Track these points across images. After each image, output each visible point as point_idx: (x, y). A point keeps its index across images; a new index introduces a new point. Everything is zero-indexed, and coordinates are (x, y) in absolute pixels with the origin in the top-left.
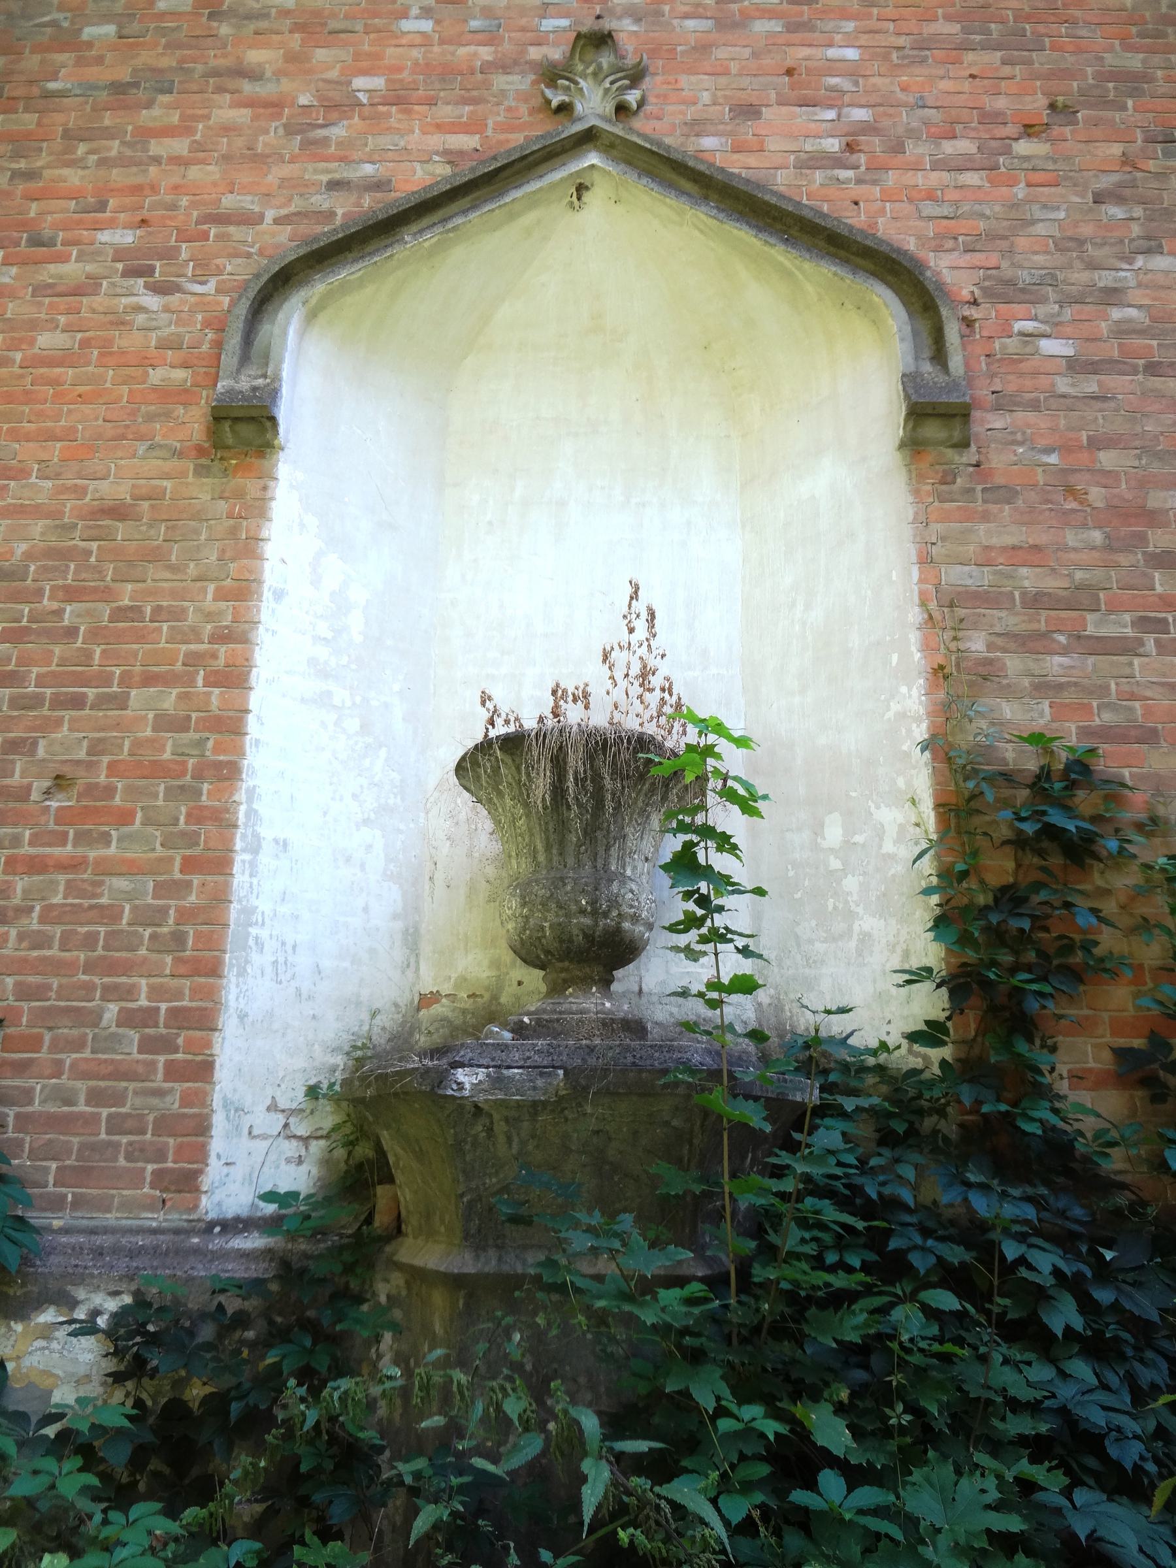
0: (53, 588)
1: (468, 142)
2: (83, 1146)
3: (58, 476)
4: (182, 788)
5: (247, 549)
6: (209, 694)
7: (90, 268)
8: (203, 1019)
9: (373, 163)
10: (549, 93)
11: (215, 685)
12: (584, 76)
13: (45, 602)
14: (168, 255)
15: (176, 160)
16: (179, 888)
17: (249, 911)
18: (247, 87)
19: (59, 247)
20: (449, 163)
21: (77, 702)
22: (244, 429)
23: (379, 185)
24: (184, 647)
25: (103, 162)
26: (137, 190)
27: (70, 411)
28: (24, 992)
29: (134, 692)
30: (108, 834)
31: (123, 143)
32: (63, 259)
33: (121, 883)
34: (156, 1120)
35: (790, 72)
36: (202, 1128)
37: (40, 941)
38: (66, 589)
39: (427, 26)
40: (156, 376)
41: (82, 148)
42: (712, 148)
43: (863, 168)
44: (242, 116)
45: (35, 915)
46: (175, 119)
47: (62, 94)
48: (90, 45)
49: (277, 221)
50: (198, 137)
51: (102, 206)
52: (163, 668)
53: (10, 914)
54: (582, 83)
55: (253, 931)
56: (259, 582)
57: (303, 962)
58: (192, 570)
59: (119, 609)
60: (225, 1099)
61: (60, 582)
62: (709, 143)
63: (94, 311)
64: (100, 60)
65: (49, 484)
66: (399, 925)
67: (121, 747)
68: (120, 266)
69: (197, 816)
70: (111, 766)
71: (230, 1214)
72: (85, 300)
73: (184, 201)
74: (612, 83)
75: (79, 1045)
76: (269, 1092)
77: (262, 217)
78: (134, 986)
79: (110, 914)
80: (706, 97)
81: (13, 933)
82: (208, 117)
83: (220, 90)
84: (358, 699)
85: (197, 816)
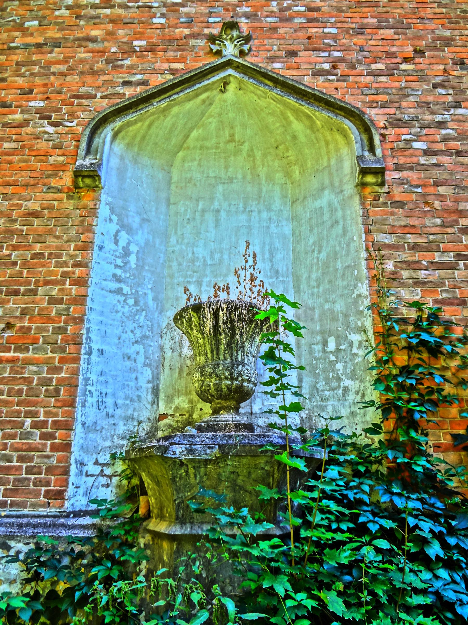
0: (7, 246)
4: (59, 328)
10: (212, 46)
14: (58, 111)
18: (91, 45)
21: (16, 292)
22: (88, 179)
23: (144, 83)
24: (61, 270)
27: (16, 174)
32: (15, 113)
38: (13, 246)
39: (163, 21)
41: (23, 69)
49: (102, 97)
51: (31, 92)
52: (52, 278)
60: (76, 459)
61: (11, 243)
64: (32, 35)
68: (38, 115)
70: (30, 319)
72: (23, 129)
75: (13, 437)
77: (96, 95)
78: (38, 411)
79: (28, 381)
83: (80, 46)
84: (133, 291)
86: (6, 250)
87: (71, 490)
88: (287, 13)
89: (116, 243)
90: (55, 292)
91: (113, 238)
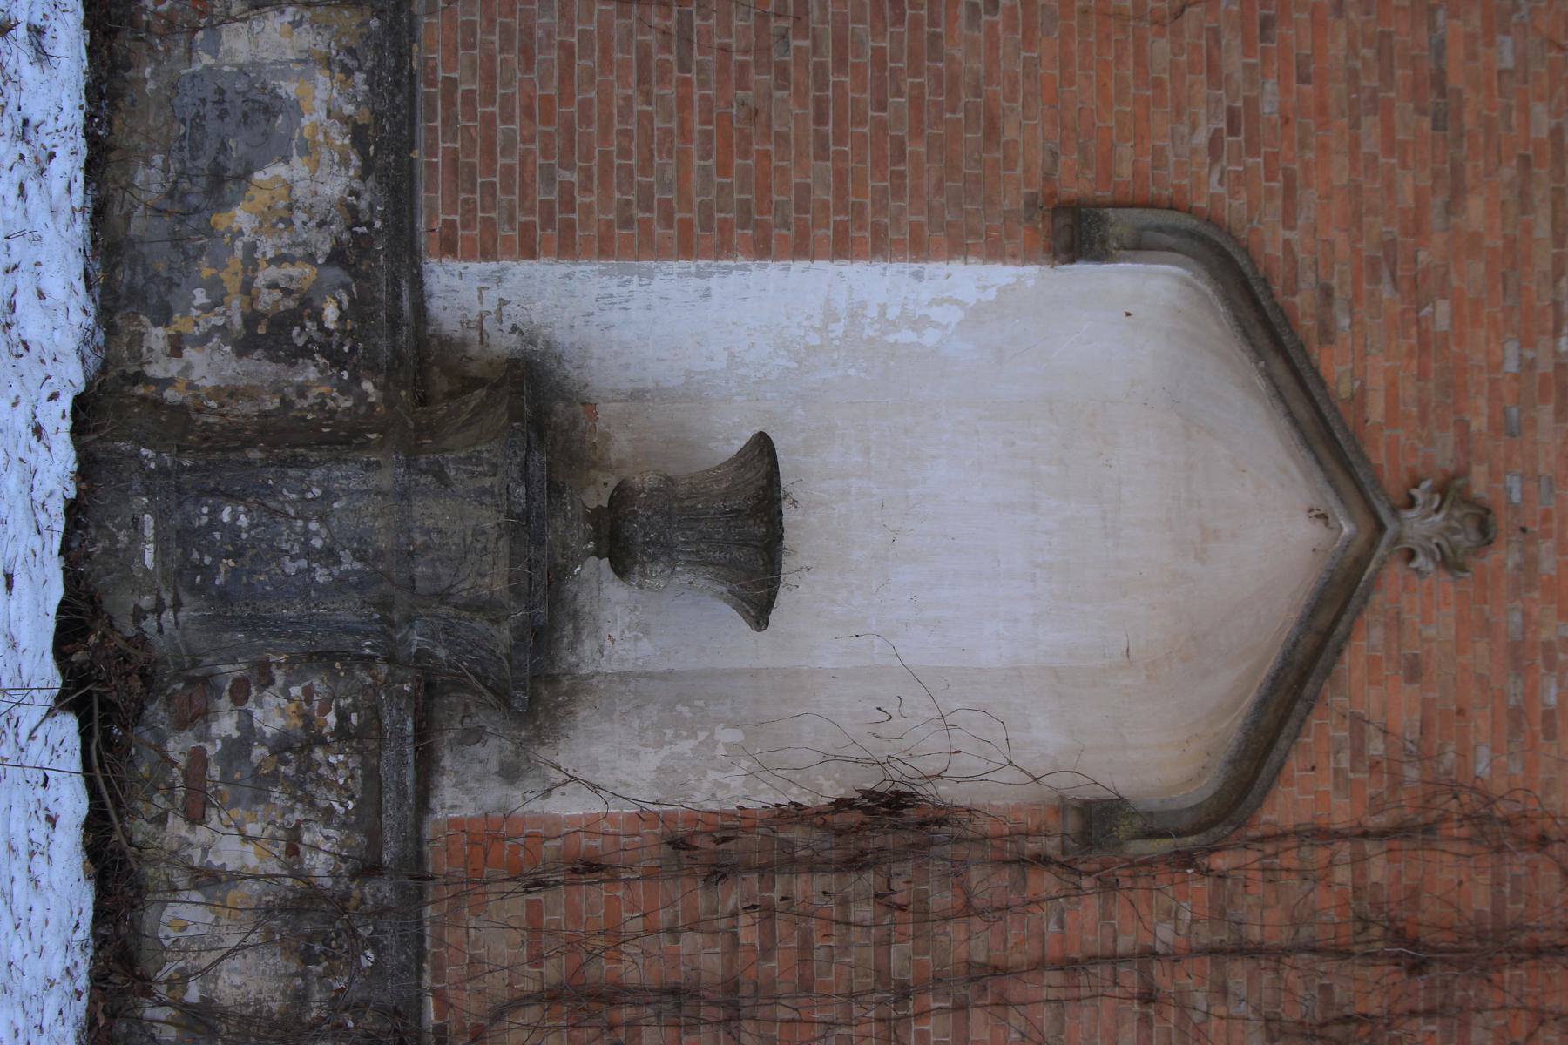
0: (921, 85)
1: (1376, 410)
2: (473, 166)
3: (1027, 76)
4: (749, 211)
5: (957, 244)
6: (827, 226)
7: (1239, 76)
8: (566, 249)
9: (1351, 325)
10: (1425, 485)
11: (836, 231)
12: (1448, 517)
13: (909, 80)
14: (1252, 148)
15: (1355, 143)
16: (668, 221)
17: (650, 275)
18: (1437, 202)
19: (1260, 45)
20: (1353, 395)
21: (820, 119)
22: (1075, 233)
23: (1327, 334)
24: (869, 201)
25: (1353, 75)
26: (1322, 109)
27: (1089, 77)
28: (585, 105)
29: (829, 164)
30: (709, 156)
31: (1375, 91)
32: (1248, 49)
33: (670, 173)
34: (492, 219)
35: (1461, 712)
36: (487, 254)
37: (625, 113)
38: (921, 96)
39: (1512, 366)
40: (1126, 150)
41: (1368, 53)
42: (1369, 640)
43: (1351, 775)
44: (1407, 198)
45: (645, 108)
46: (1400, 136)
47: (1432, 27)
48: (1490, 44)
49: (1287, 243)
50: (1382, 160)
51: (1304, 79)
52: (850, 185)
53: (645, 87)
54: (1441, 515)
55: (635, 279)
56: (926, 260)
57: (615, 316)
58: (938, 201)
59: (903, 143)
60: (507, 269)
61: (927, 90)
62: (1377, 634)
63: (1191, 86)
64: (1472, 56)
65: (1019, 70)
66: (650, 385)
67: (782, 159)
68: (1239, 104)
69: (725, 227)
70: (767, 154)
71: (425, 279)
72: (1204, 76)
73: (1310, 155)
74: (1438, 545)
75: (546, 153)
76: (514, 299)
77: (1292, 228)
78: (591, 191)
79: (646, 166)
80: (1431, 632)
81: (630, 92)
82: (1404, 166)
83: (1436, 176)
84: (837, 342)
85: (725, 227)
86: (913, 85)
87: (458, 266)
88: (1539, 660)
89: (935, 302)
90: (818, 194)
91: (946, 295)
